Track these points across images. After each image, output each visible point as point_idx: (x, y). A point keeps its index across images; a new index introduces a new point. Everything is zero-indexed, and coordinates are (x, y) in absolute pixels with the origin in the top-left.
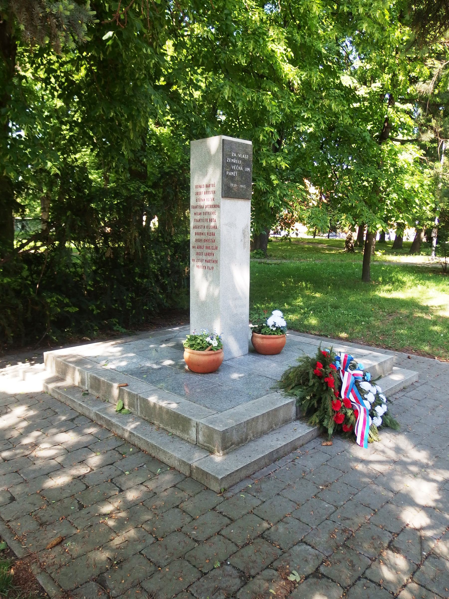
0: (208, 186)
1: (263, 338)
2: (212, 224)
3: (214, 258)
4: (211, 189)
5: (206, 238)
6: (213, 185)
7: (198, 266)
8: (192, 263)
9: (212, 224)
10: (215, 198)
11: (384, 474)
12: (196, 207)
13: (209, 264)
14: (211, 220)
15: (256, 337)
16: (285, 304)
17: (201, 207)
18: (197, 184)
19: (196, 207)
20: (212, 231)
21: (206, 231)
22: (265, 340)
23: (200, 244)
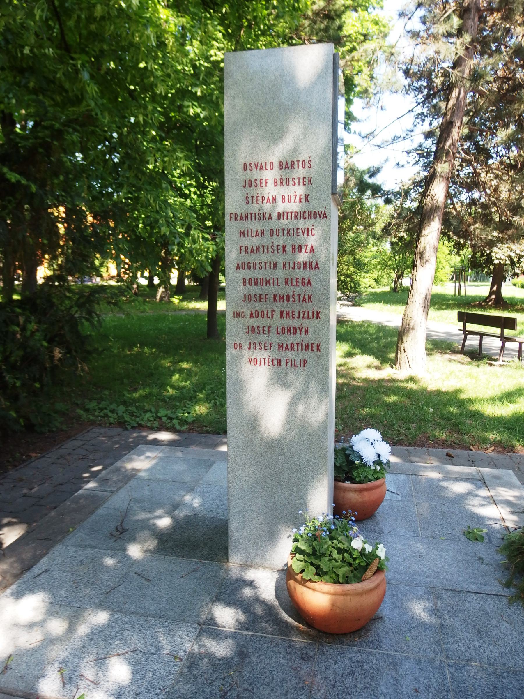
0: (287, 165)
1: (361, 491)
2: (303, 257)
3: (310, 339)
4: (300, 172)
5: (282, 292)
6: (307, 164)
7: (253, 361)
8: (230, 353)
9: (303, 257)
10: (313, 194)
11: (372, 622)
12: (244, 217)
13: (291, 355)
14: (296, 249)
15: (345, 490)
16: (168, 388)
17: (263, 217)
18: (248, 160)
19: (244, 217)
20: (306, 274)
21: (280, 274)
22: (365, 493)
23: (259, 307)
